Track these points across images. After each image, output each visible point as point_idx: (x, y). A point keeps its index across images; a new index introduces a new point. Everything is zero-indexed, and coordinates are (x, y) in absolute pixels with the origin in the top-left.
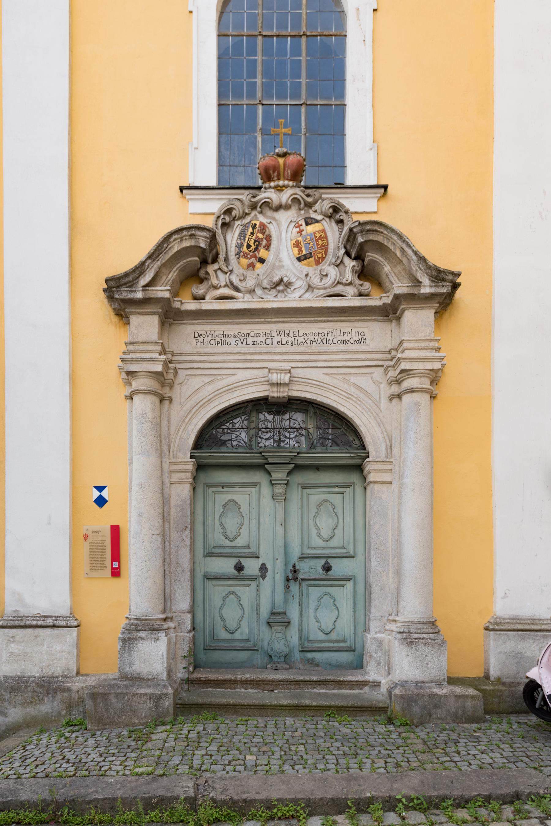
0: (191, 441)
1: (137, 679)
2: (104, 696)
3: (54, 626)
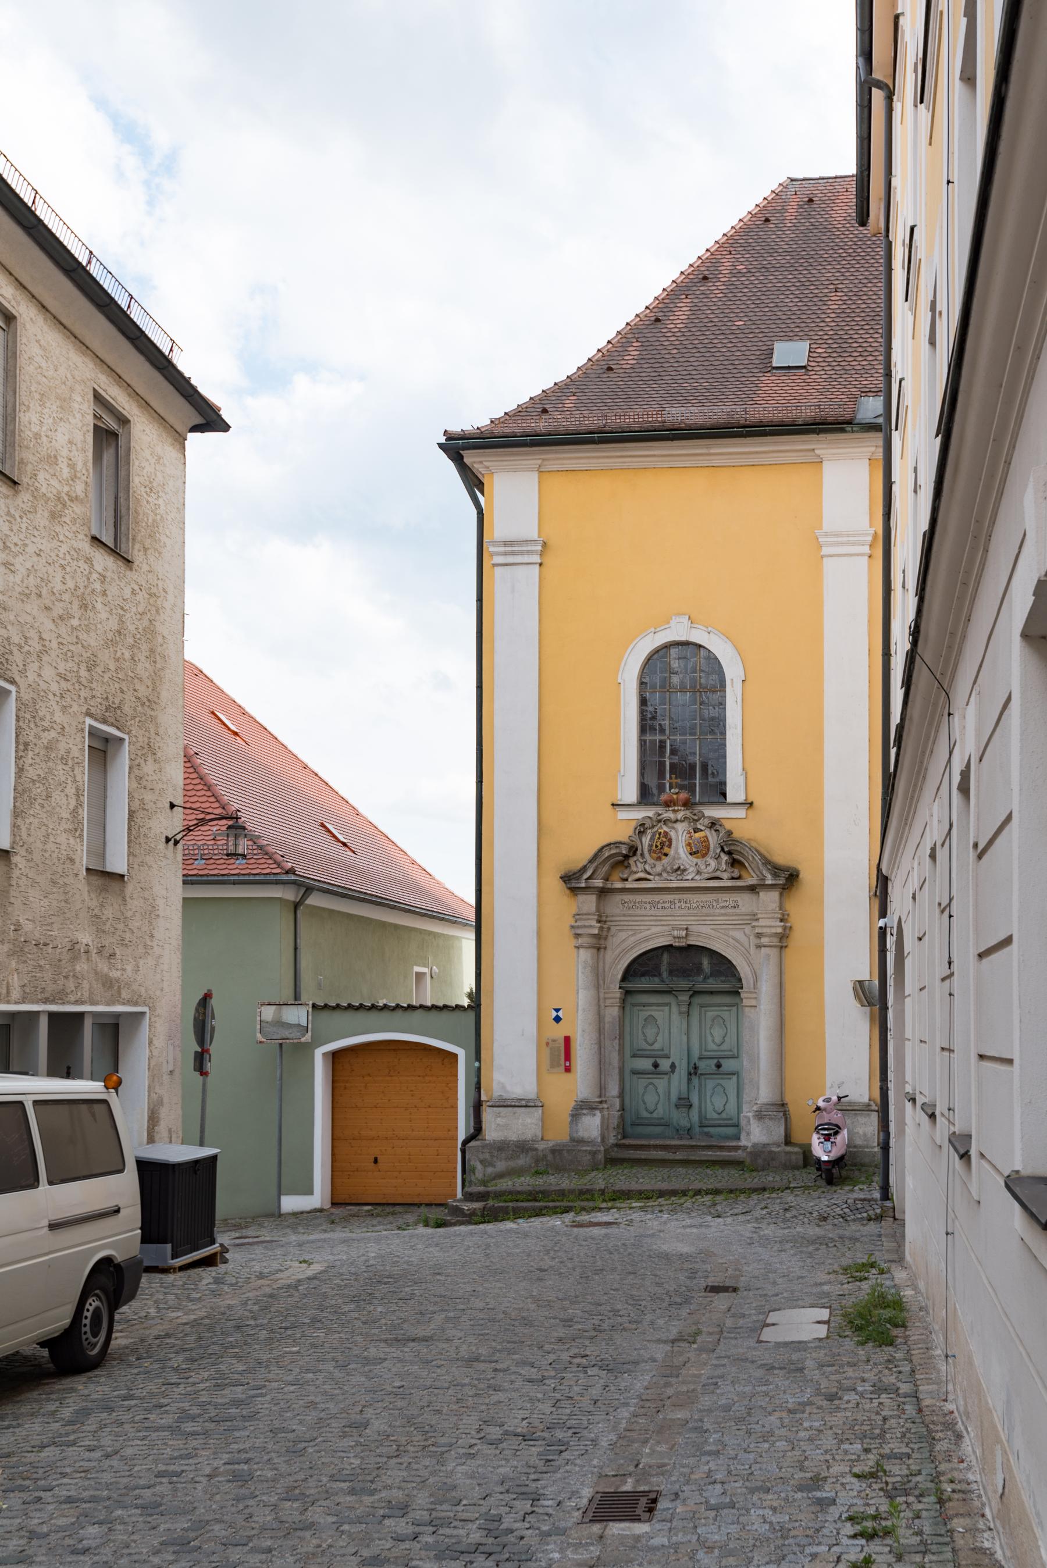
0: (620, 976)
1: (581, 1141)
2: (560, 1151)
3: (526, 1106)
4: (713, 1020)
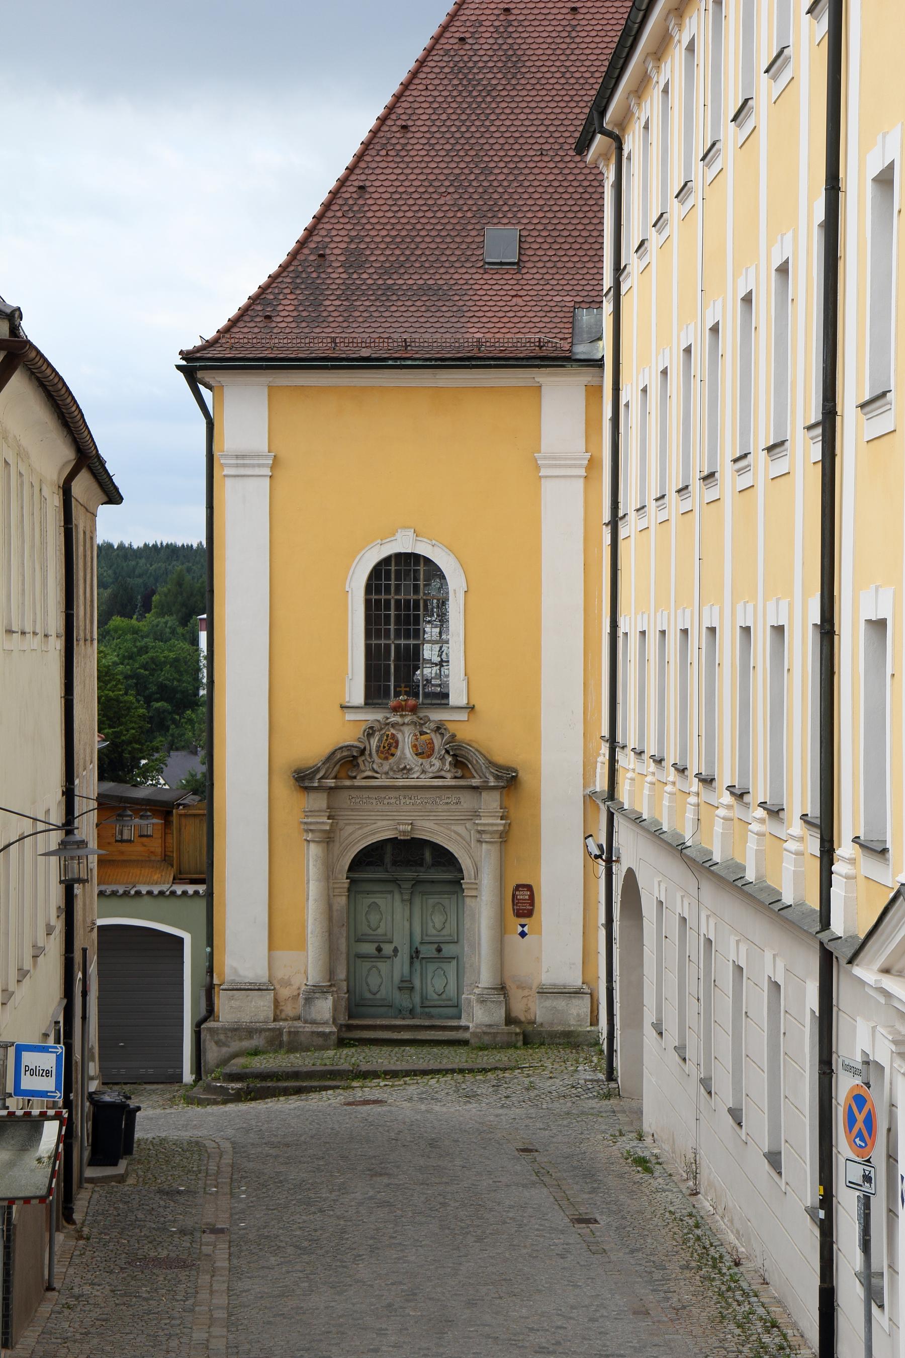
0: (347, 867)
4: (434, 907)
